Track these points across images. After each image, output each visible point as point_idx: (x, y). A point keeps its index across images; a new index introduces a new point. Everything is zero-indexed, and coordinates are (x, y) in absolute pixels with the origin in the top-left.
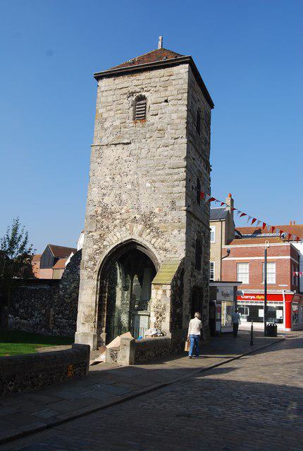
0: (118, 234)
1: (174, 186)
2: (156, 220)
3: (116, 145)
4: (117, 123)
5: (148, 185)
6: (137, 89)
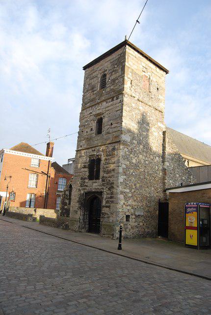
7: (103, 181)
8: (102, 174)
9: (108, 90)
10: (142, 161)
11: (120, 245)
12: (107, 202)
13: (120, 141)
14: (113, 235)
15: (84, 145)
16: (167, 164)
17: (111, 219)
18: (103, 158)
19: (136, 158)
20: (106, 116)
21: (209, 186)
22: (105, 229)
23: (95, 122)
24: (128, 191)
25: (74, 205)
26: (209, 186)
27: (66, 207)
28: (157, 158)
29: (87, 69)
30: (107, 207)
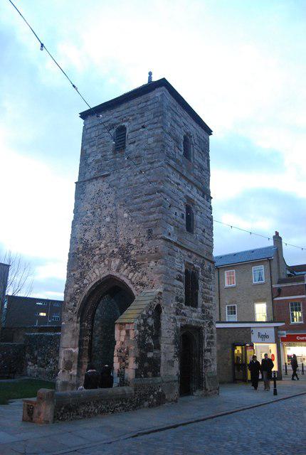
0: (97, 271)
1: (150, 213)
2: (133, 252)
3: (96, 178)
4: (99, 157)
5: (126, 215)
6: (116, 120)
7: (203, 311)
8: (200, 300)
12: (208, 343)
27: (150, 355)
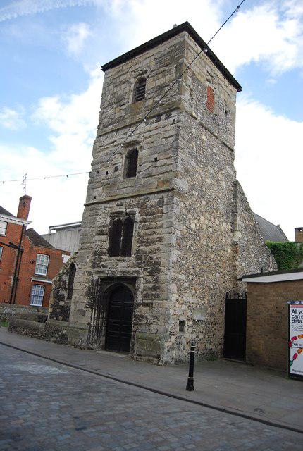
7: (138, 258)
8: (135, 246)
9: (150, 102)
10: (205, 227)
11: (191, 382)
12: (146, 296)
13: (173, 189)
14: (158, 357)
15: (100, 196)
16: (238, 235)
17: (154, 328)
18: (138, 217)
19: (196, 221)
20: (146, 146)
21: (299, 276)
22: (142, 344)
23: (124, 156)
24: (183, 277)
25: (79, 299)
26: (299, 276)
27: (62, 303)
28: (225, 224)
29: (110, 70)
30: (145, 305)
